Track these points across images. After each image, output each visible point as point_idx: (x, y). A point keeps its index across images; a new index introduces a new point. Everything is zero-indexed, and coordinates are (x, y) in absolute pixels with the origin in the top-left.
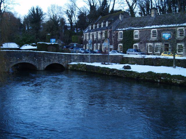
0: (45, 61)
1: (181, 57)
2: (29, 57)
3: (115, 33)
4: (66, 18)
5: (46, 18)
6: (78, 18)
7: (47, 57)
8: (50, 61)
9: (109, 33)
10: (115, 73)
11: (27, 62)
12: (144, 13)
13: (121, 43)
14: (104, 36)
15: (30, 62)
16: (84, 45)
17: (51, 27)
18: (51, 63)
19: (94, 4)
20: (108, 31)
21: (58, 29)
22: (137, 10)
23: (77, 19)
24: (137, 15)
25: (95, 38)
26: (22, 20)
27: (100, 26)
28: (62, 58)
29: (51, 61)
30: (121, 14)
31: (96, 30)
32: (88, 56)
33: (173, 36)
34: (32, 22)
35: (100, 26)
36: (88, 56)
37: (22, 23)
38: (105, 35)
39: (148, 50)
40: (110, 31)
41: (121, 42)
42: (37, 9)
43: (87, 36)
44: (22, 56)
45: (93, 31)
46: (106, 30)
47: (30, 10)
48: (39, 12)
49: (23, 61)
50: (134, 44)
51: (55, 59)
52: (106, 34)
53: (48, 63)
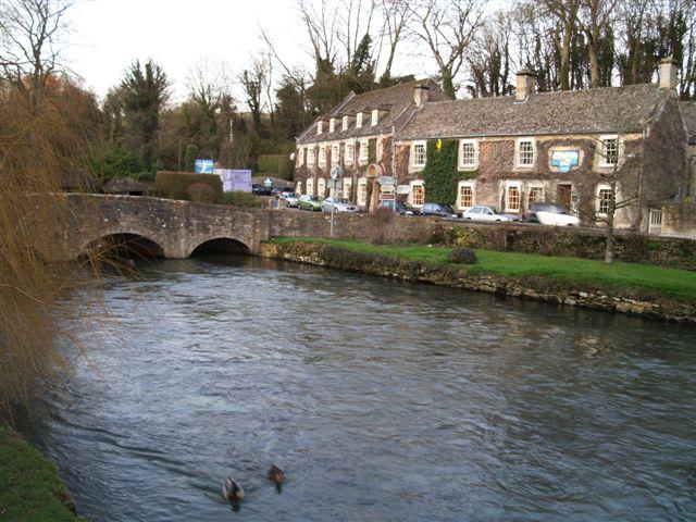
0: (191, 231)
1: (670, 271)
2: (140, 215)
3: (400, 147)
5: (177, 96)
6: (277, 96)
8: (206, 230)
9: (381, 147)
10: (422, 275)
11: (132, 231)
12: (484, 89)
13: (419, 178)
14: (363, 157)
16: (299, 183)
17: (193, 121)
18: (212, 236)
19: (328, 55)
20: (379, 142)
21: (213, 129)
22: (463, 77)
23: (275, 100)
24: (462, 94)
25: (337, 160)
26: (101, 98)
27: (352, 124)
28: (245, 222)
29: (209, 229)
30: (422, 87)
31: (339, 135)
32: (327, 218)
33: (585, 160)
34: (132, 107)
35: (352, 124)
36: (327, 218)
37: (100, 107)
38: (369, 150)
39: (507, 203)
40: (384, 141)
41: (419, 175)
42: (148, 66)
43: (309, 153)
44: (119, 212)
45: (329, 140)
46: (373, 137)
48: (155, 75)
49: (122, 227)
50: (462, 184)
51: (223, 224)
52: (372, 148)
53: (201, 238)
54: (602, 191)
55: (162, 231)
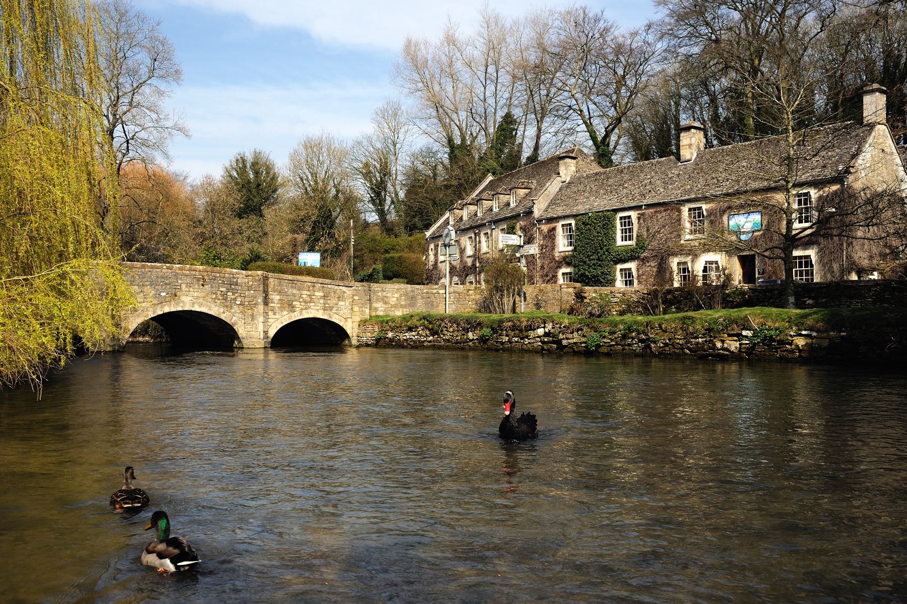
4: (361, 188)
7: (280, 293)
8: (292, 308)
11: (197, 308)
15: (210, 309)
18: (296, 316)
41: (566, 261)
47: (229, 168)
54: (679, 264)
55: (235, 308)
